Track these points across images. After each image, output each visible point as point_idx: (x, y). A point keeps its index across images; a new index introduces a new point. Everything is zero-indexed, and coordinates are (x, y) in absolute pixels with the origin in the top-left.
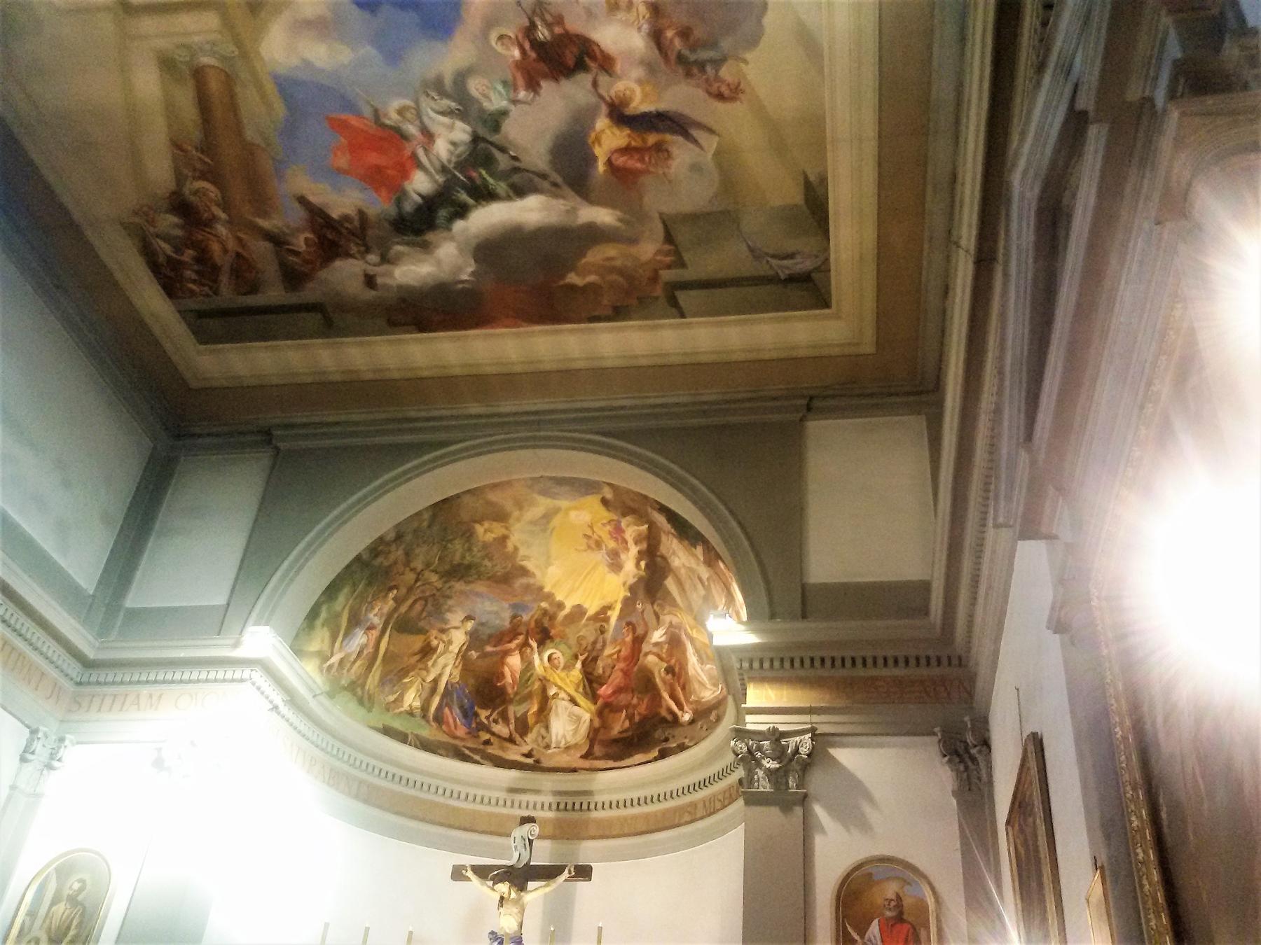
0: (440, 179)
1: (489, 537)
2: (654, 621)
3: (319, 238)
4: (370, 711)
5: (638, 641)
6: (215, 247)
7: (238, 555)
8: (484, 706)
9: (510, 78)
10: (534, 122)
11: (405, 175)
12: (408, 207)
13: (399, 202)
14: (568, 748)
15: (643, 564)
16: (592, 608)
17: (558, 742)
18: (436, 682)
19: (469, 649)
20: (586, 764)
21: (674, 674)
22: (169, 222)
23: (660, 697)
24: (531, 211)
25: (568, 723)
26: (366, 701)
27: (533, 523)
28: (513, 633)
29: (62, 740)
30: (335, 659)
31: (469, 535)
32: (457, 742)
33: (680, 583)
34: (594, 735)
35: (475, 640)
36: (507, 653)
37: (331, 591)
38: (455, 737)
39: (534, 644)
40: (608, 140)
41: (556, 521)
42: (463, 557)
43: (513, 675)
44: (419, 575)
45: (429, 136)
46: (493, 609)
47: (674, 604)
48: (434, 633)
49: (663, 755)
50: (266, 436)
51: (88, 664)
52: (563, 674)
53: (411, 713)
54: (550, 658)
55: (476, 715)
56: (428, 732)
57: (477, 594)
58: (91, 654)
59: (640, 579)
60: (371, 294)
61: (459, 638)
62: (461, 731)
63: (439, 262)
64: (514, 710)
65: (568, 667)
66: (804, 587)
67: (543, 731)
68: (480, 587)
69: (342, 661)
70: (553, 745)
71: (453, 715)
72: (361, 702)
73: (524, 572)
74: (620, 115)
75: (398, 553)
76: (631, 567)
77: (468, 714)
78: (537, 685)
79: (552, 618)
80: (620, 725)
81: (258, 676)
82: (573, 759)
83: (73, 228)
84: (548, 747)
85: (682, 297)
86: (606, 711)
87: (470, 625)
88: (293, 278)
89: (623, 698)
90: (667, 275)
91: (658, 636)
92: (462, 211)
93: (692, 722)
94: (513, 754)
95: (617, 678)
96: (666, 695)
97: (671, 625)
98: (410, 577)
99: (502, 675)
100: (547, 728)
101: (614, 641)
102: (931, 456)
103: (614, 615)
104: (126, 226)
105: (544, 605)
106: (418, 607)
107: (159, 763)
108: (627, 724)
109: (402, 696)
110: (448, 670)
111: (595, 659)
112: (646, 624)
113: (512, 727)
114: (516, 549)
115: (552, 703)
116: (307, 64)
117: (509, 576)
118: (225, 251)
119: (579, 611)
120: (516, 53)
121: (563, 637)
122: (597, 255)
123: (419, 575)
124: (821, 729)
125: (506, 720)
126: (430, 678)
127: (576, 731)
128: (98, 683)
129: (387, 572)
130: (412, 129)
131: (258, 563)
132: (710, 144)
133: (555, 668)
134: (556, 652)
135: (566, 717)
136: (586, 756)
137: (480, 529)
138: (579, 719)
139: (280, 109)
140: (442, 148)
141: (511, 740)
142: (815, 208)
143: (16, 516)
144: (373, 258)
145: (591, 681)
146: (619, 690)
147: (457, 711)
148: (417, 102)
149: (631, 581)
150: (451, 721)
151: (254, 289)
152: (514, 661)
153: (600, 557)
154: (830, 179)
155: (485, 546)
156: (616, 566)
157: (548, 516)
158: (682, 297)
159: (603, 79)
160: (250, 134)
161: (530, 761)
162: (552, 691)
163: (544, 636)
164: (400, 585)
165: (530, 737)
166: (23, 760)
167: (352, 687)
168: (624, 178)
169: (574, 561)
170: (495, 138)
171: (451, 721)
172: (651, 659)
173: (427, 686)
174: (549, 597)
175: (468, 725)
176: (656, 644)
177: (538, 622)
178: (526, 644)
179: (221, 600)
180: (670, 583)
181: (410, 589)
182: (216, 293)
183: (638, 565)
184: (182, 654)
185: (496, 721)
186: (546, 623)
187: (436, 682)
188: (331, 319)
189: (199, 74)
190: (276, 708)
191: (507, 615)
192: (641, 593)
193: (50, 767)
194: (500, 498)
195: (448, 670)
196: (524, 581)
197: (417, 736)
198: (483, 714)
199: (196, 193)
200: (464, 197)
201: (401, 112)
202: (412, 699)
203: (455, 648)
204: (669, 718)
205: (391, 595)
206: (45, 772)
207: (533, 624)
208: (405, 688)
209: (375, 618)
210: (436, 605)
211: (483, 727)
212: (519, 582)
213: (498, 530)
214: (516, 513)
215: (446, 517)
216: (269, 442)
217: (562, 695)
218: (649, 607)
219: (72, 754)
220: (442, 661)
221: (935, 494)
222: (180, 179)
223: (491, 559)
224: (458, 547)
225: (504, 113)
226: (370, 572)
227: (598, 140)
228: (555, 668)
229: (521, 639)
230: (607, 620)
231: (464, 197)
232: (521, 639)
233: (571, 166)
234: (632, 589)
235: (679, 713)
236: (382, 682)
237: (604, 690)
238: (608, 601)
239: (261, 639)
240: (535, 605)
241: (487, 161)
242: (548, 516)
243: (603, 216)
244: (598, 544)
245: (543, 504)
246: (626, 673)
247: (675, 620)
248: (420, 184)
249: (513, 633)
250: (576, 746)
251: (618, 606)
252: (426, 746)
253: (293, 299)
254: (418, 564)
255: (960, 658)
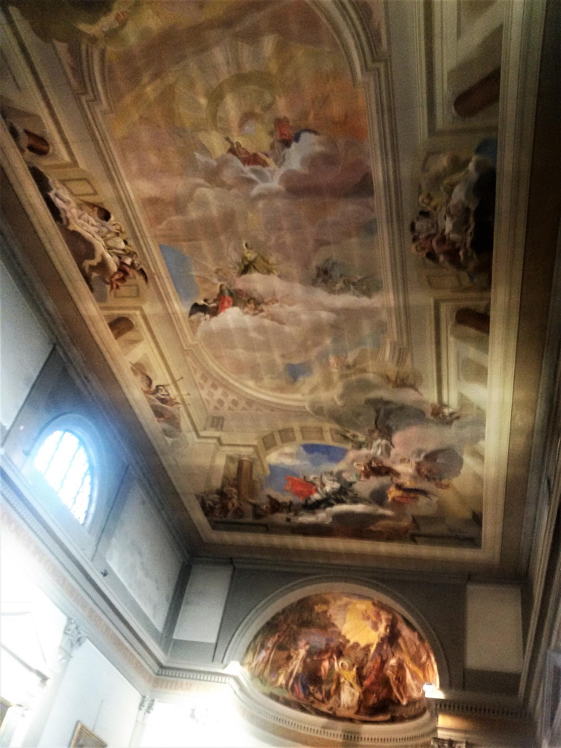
0: (324, 496)
1: (320, 610)
2: (392, 655)
3: (272, 507)
4: (265, 685)
5: (384, 662)
6: (230, 505)
7: (219, 620)
8: (312, 685)
9: (359, 474)
10: (365, 486)
11: (311, 493)
12: (309, 502)
13: (306, 501)
14: (348, 708)
15: (388, 631)
16: (363, 644)
17: (344, 705)
18: (291, 673)
19: (306, 658)
20: (356, 717)
21: (399, 681)
22: (216, 497)
23: (392, 691)
24: (359, 508)
25: (349, 696)
26: (263, 681)
27: (340, 606)
28: (326, 651)
29: (153, 701)
30: (253, 665)
31: (312, 610)
32: (300, 701)
33: (405, 642)
34: (360, 703)
35: (309, 653)
36: (324, 660)
37: (256, 637)
38: (299, 699)
39: (335, 658)
40: (393, 493)
41: (350, 607)
42: (308, 618)
43: (325, 670)
44: (288, 625)
45: (323, 485)
46: (318, 640)
47: (401, 650)
48: (292, 650)
49: (393, 720)
50: (231, 561)
51: (161, 666)
52: (348, 673)
53: (281, 687)
54: (342, 664)
55: (308, 688)
56: (288, 695)
57: (312, 634)
58: (164, 663)
59: (386, 636)
60: (287, 523)
61: (302, 652)
62: (302, 695)
63: (317, 518)
64: (325, 687)
65: (350, 669)
66: (464, 669)
67: (337, 698)
68: (313, 630)
69: (256, 665)
70: (342, 706)
71: (299, 688)
72: (262, 681)
73: (333, 625)
74: (399, 487)
75: (282, 618)
76: (382, 629)
77: (305, 687)
78: (335, 677)
79: (344, 646)
80: (373, 700)
81: (232, 681)
82: (350, 713)
83: (176, 494)
84: (339, 706)
85: (417, 538)
86: (366, 693)
87: (307, 647)
88: (257, 516)
89: (375, 688)
90: (411, 531)
91: (393, 662)
92: (331, 505)
93: (407, 705)
94: (324, 708)
95: (372, 677)
96: (395, 690)
97: (399, 659)
98: (285, 626)
99: (320, 670)
100: (339, 698)
101: (372, 660)
102: (523, 626)
103: (373, 649)
104: (197, 497)
105: (341, 640)
106: (287, 639)
107: (193, 716)
108: (376, 700)
109: (277, 680)
110: (297, 667)
111: (363, 668)
112: (387, 656)
113: (324, 695)
114: (331, 616)
115: (342, 685)
116: (284, 464)
117: (326, 626)
118: (233, 505)
119: (356, 645)
120: (363, 469)
121: (349, 656)
122: (382, 523)
123: (288, 625)
124: (470, 741)
125: (321, 692)
126: (289, 671)
127: (352, 700)
128: (165, 675)
129: (277, 625)
130: (318, 483)
131: (229, 624)
132: (435, 499)
133: (344, 669)
134: (345, 662)
135: (207, 391)
136: (358, 712)
137: (316, 607)
138: (353, 695)
139: (268, 472)
140: (328, 488)
141: (323, 701)
142: (477, 519)
143: (137, 600)
144: (292, 514)
145: (360, 678)
146: (373, 684)
147: (300, 686)
148: (321, 477)
149: (382, 635)
150: (297, 691)
151: (241, 517)
152: (326, 664)
153: (368, 624)
154: (483, 513)
155: (318, 614)
156: (375, 627)
157: (346, 605)
158: (417, 538)
159: (395, 478)
160: (254, 477)
161: (330, 712)
162: (342, 680)
163: (340, 654)
164: (280, 632)
165: (332, 701)
166: (140, 709)
167: (258, 676)
168: (397, 504)
169: (358, 625)
170: (350, 488)
171: (297, 691)
172: (389, 672)
173: (288, 675)
174: (344, 637)
175: (305, 693)
176: (392, 666)
177: (338, 647)
178: (331, 657)
179: (213, 640)
180: (400, 641)
181: (284, 632)
182: (225, 517)
183: (386, 629)
184: (202, 669)
185: (317, 692)
186: (341, 648)
187: (291, 673)
188: (268, 529)
189: (241, 462)
190: (235, 692)
191: (324, 643)
192: (386, 641)
193: (148, 712)
194: (329, 597)
195: (297, 667)
196: (332, 629)
197: (284, 698)
198: (311, 688)
199: (228, 490)
200: (333, 502)
201: (315, 478)
202: (282, 680)
203: (300, 657)
204: (396, 701)
205: (277, 635)
206: (146, 714)
207: (335, 649)
208: (279, 675)
209: (270, 645)
210: (294, 639)
211: (310, 694)
212: (330, 630)
213: (325, 607)
214: (333, 602)
215: (304, 605)
216: (232, 563)
217: (347, 682)
218: (389, 649)
219: (157, 705)
220: (294, 663)
221: (524, 653)
222: (223, 486)
223: (319, 619)
224: (306, 615)
225: (355, 483)
226: (271, 627)
227: (390, 493)
228: (344, 669)
229: (329, 654)
230: (369, 651)
231: (333, 502)
232: (329, 654)
233: (378, 497)
234: (382, 639)
235: (401, 701)
236: (271, 671)
237: (366, 683)
238: (371, 641)
239: (238, 669)
240: (336, 640)
241: (345, 494)
242: (346, 605)
243: (388, 512)
244: (368, 618)
245: (345, 600)
246: (377, 677)
247: (401, 657)
248: (316, 496)
249: (326, 651)
250: (352, 707)
251: (375, 646)
252: (287, 703)
253: (256, 521)
254: (289, 621)
255: (530, 715)
